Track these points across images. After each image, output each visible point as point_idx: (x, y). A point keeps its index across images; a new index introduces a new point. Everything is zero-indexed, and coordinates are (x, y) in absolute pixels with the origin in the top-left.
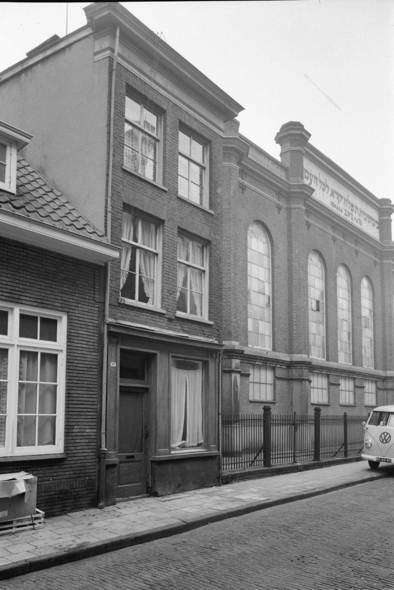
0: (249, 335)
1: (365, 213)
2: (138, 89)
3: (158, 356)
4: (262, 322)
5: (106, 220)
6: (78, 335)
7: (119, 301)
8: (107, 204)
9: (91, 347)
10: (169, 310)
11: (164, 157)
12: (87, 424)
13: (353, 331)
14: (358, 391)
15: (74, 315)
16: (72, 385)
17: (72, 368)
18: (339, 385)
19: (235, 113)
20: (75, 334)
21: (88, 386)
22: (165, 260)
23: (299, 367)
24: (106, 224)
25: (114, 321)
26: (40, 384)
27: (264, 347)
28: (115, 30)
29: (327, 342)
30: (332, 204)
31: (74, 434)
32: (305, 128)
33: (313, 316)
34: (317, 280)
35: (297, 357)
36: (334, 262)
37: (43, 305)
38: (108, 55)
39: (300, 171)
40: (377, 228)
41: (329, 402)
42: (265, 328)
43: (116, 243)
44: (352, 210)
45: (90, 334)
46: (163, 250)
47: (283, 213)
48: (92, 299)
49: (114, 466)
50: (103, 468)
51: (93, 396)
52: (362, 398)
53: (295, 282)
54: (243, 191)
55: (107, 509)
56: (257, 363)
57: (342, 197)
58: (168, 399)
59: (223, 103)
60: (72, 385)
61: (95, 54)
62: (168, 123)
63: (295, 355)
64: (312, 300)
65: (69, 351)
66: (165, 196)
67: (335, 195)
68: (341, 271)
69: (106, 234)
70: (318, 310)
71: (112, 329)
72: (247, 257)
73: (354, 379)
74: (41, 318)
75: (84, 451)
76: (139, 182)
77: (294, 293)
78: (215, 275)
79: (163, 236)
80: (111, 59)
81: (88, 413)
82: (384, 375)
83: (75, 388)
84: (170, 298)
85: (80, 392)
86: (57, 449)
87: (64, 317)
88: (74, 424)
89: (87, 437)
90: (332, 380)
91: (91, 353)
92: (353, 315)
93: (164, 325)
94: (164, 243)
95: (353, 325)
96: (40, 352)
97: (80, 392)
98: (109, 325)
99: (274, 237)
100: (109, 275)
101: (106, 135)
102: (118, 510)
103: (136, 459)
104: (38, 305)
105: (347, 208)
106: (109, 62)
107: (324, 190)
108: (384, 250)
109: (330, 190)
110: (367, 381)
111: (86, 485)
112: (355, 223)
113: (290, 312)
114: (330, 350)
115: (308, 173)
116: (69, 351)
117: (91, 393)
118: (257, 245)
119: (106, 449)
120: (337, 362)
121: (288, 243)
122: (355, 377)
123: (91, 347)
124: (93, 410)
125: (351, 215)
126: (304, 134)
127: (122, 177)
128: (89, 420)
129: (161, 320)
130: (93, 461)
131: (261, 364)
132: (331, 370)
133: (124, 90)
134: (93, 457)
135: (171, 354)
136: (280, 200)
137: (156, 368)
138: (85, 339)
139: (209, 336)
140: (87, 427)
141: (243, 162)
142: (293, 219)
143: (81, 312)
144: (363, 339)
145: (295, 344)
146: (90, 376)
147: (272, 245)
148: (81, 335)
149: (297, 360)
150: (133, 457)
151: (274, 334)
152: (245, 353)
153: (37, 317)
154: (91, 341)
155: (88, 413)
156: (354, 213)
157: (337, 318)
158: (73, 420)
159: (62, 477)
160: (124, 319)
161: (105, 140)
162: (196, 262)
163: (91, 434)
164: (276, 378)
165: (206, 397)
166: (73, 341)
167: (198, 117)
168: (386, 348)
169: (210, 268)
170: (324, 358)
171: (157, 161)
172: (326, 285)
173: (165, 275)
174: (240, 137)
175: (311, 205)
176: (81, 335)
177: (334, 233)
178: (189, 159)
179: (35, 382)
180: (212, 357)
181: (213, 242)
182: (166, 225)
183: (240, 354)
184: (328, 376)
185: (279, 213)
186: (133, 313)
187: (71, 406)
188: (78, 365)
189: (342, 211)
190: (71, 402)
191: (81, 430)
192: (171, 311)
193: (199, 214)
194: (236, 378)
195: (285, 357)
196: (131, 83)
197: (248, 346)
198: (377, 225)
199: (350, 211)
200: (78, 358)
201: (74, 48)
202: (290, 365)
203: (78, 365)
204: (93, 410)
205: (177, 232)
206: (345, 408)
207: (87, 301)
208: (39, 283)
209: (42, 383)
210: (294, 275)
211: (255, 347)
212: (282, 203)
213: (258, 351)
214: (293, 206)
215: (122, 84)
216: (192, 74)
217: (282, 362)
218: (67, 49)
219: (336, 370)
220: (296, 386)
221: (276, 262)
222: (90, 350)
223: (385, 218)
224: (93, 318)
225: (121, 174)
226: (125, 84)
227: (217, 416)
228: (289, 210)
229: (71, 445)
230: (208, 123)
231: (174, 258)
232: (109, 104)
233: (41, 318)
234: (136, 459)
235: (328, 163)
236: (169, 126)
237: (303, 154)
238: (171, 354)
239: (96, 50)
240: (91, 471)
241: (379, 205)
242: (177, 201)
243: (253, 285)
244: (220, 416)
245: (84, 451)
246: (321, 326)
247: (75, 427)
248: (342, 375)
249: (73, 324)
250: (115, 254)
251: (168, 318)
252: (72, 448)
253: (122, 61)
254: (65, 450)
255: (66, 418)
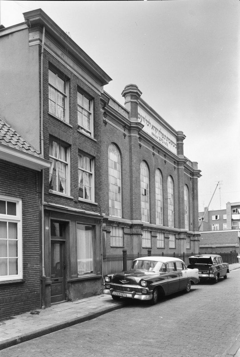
0: (110, 208)
1: (169, 140)
2: (55, 65)
3: (70, 222)
4: (117, 202)
5: (41, 144)
6: (28, 212)
7: (49, 192)
8: (41, 135)
9: (35, 218)
10: (75, 197)
11: (70, 107)
12: (34, 262)
13: (163, 207)
14: (166, 240)
15: (25, 200)
16: (26, 240)
17: (26, 230)
18: (156, 237)
19: (107, 82)
20: (27, 211)
21: (34, 241)
22: (72, 168)
23: (137, 227)
24: (41, 146)
25: (46, 203)
26: (9, 240)
27: (118, 216)
28: (42, 28)
29: (150, 213)
30: (152, 133)
31: (28, 268)
32: (139, 88)
33: (143, 198)
34: (144, 177)
35: (135, 222)
36: (154, 167)
37: (9, 195)
38: (38, 43)
39: (136, 115)
40: (176, 148)
41: (151, 247)
42: (118, 206)
43: (47, 158)
44: (163, 137)
45: (34, 211)
46: (71, 162)
47: (176, 170)
48: (35, 191)
49: (49, 285)
50: (44, 285)
51: (37, 246)
52: (168, 244)
53: (134, 179)
54: (105, 125)
55: (47, 309)
56: (114, 225)
57: (157, 130)
58: (76, 247)
59: (101, 75)
60: (26, 240)
61: (30, 42)
62: (72, 86)
63: (134, 220)
64: (143, 189)
65: (24, 221)
66: (71, 131)
67: (154, 128)
68: (157, 173)
69: (41, 153)
70: (145, 195)
71: (47, 208)
72: (108, 164)
73: (164, 233)
74: (7, 202)
75: (33, 277)
76: (57, 122)
77: (133, 185)
78: (97, 176)
79: (71, 153)
80: (40, 47)
81: (35, 256)
82: (193, 233)
83: (27, 242)
84: (75, 190)
85: (31, 244)
86: (19, 276)
87: (20, 201)
88: (27, 262)
89: (35, 270)
90: (153, 234)
91: (35, 222)
92: (163, 197)
93: (72, 205)
94: (71, 158)
95: (163, 203)
96: (8, 221)
97: (31, 244)
98: (45, 206)
99: (122, 152)
100: (44, 177)
101: (38, 93)
102: (53, 309)
103: (59, 281)
104: (7, 194)
105: (160, 136)
106: (39, 48)
107: (148, 125)
108: (179, 161)
109: (151, 125)
110: (170, 234)
111: (35, 296)
112: (164, 145)
113: (131, 196)
114: (152, 218)
115: (140, 115)
116: (24, 221)
117: (36, 244)
118: (113, 156)
119: (45, 276)
120: (156, 224)
121: (129, 156)
122: (164, 232)
123: (35, 218)
124: (38, 254)
125: (162, 140)
126: (138, 92)
127: (48, 119)
128: (36, 260)
129: (71, 203)
130: (38, 283)
131: (116, 225)
132: (152, 229)
133: (47, 66)
134: (39, 281)
135: (77, 222)
136: (141, 141)
137: (69, 230)
138: (32, 214)
139: (96, 211)
140: (35, 264)
141: (106, 108)
142: (132, 142)
143: (29, 198)
144: (169, 211)
145: (134, 215)
146: (35, 235)
147: (121, 157)
148: (30, 212)
149: (135, 223)
150: (57, 280)
151: (123, 209)
152: (109, 220)
153: (5, 201)
154: (35, 215)
155: (35, 256)
156: (163, 139)
157: (155, 199)
158: (28, 260)
159: (23, 292)
160: (52, 202)
161: (38, 96)
162: (88, 169)
163: (37, 268)
164: (124, 234)
165: (94, 245)
166: (26, 215)
167: (87, 83)
168: (180, 216)
169: (95, 173)
170: (148, 222)
171: (65, 109)
172: (150, 180)
173: (72, 177)
174: (104, 93)
175: (152, 142)
176: (30, 212)
177: (124, 131)
178: (82, 108)
179: (6, 239)
180: (97, 223)
181: (96, 158)
182: (72, 147)
183: (106, 220)
184: (151, 232)
185: (125, 138)
186: (56, 199)
187: (26, 252)
188: (29, 229)
189: (157, 138)
190: (26, 250)
191: (31, 266)
192: (76, 197)
193: (89, 141)
194: (104, 234)
195: (129, 222)
196: (51, 61)
197: (109, 216)
198: (176, 146)
199: (162, 138)
200: (29, 225)
201: (14, 34)
202: (132, 226)
203: (29, 229)
204: (38, 254)
205: (78, 152)
206: (172, 249)
207: (32, 192)
208: (7, 182)
209: (9, 239)
210: (133, 175)
211: (113, 216)
212: (126, 133)
213: (115, 218)
214: (132, 134)
215: (46, 61)
216: (84, 57)
217: (127, 225)
218: (10, 36)
219: (155, 229)
220: (135, 238)
221: (124, 167)
222: (35, 220)
223: (180, 142)
224: (36, 202)
225: (48, 117)
226: (48, 62)
227: (100, 256)
228: (130, 136)
229: (27, 274)
230: (92, 87)
231: (77, 167)
232: (39, 74)
233: (7, 202)
234: (59, 281)
235: (150, 110)
236: (72, 88)
237: (137, 104)
238: (77, 222)
239: (30, 39)
240: (37, 288)
241: (177, 135)
242: (77, 133)
243: (111, 180)
244: (102, 256)
245: (33, 277)
246: (147, 204)
247: (28, 264)
248: (158, 231)
249: (25, 205)
250: (47, 165)
251: (75, 201)
252: (27, 276)
253: (46, 47)
254: (23, 277)
255: (23, 259)
